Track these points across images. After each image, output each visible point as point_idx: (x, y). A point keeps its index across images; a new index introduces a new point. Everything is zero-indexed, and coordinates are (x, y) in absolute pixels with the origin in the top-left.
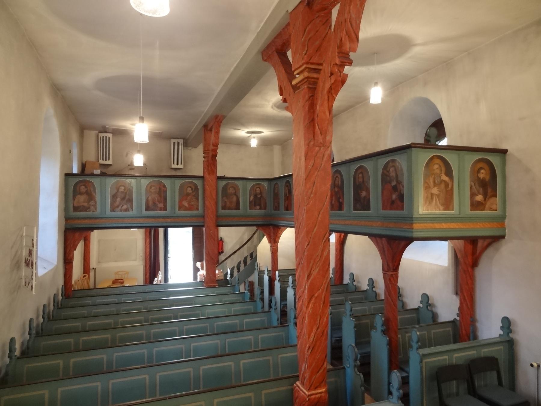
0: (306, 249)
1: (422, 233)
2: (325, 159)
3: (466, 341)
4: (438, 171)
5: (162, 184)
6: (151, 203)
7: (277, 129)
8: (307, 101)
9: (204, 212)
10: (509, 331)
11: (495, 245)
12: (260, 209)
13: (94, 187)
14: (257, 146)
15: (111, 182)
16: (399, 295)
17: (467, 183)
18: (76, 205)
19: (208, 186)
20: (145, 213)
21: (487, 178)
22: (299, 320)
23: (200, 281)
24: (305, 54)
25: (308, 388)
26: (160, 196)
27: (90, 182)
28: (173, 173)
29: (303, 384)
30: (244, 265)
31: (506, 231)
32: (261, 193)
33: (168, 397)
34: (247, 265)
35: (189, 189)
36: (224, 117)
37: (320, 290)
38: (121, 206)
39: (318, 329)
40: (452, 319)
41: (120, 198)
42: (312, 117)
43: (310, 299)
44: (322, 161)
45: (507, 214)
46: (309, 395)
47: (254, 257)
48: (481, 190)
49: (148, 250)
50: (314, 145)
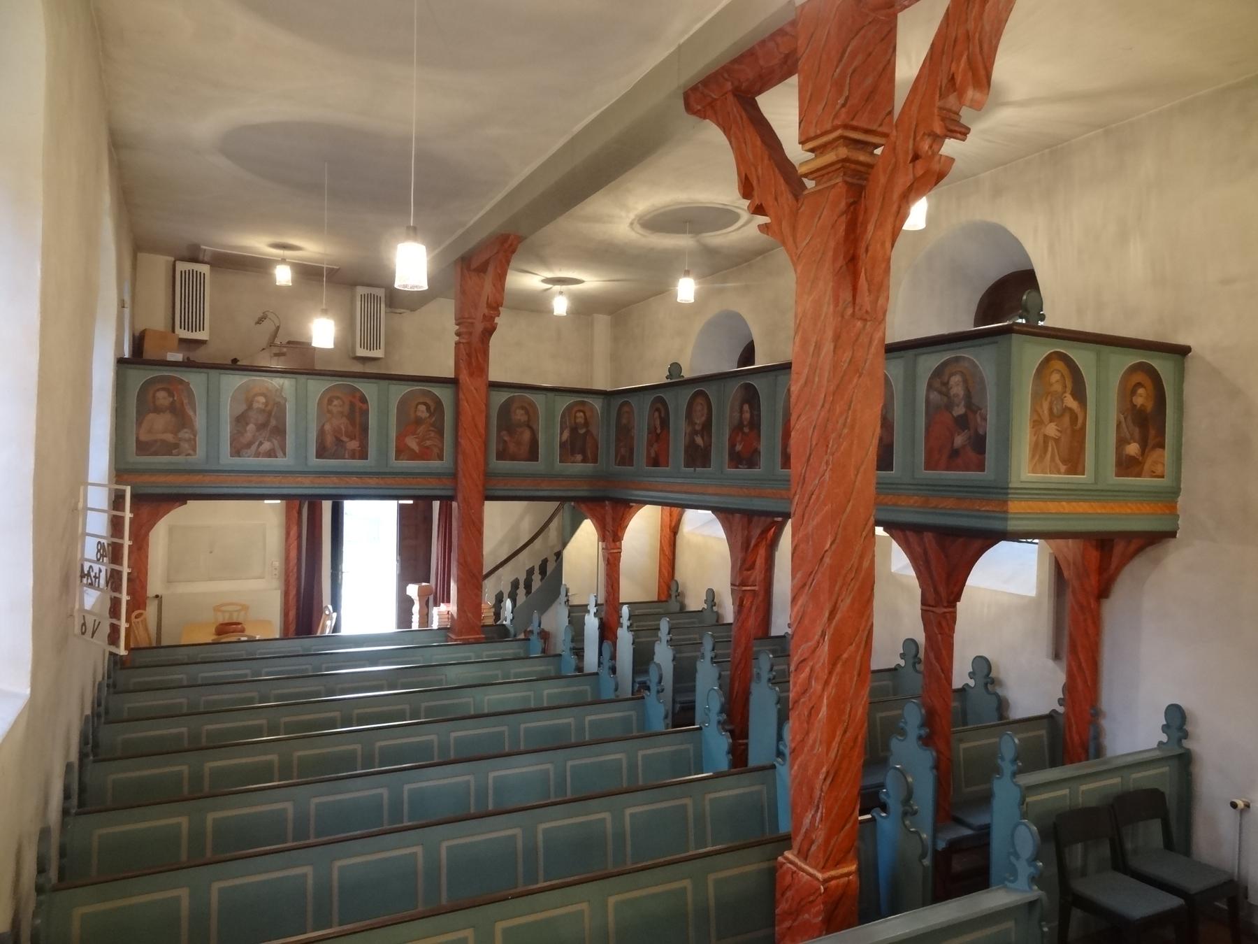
0: (829, 554)
1: (1025, 522)
2: (873, 350)
3: (1080, 761)
4: (1058, 388)
5: (358, 395)
6: (329, 439)
7: (596, 279)
8: (842, 215)
9: (456, 463)
10: (1180, 734)
11: (1151, 552)
12: (584, 460)
13: (190, 394)
14: (567, 312)
15: (233, 383)
16: (917, 660)
17: (1112, 415)
18: (143, 438)
19: (467, 402)
20: (314, 462)
21: (1150, 406)
22: (797, 712)
23: (439, 629)
24: (843, 106)
25: (822, 864)
26: (353, 422)
27: (181, 382)
28: (358, 368)
29: (803, 855)
30: (524, 591)
31: (1179, 522)
32: (586, 424)
33: (510, 895)
34: (533, 591)
35: (422, 408)
36: (520, 239)
37: (854, 645)
38: (257, 443)
39: (845, 732)
40: (1046, 711)
41: (256, 425)
42: (851, 252)
43: (833, 664)
44: (868, 354)
45: (1182, 486)
46: (826, 881)
47: (548, 574)
48: (1137, 431)
49: (293, 554)
50: (853, 315)
